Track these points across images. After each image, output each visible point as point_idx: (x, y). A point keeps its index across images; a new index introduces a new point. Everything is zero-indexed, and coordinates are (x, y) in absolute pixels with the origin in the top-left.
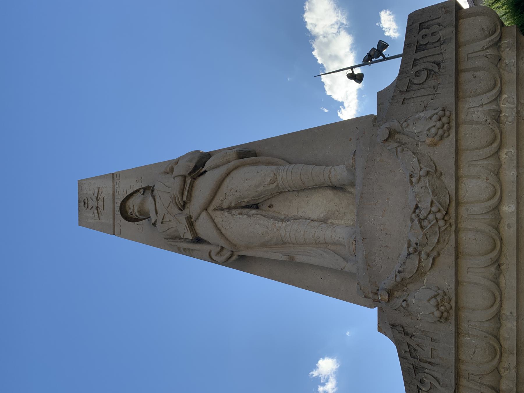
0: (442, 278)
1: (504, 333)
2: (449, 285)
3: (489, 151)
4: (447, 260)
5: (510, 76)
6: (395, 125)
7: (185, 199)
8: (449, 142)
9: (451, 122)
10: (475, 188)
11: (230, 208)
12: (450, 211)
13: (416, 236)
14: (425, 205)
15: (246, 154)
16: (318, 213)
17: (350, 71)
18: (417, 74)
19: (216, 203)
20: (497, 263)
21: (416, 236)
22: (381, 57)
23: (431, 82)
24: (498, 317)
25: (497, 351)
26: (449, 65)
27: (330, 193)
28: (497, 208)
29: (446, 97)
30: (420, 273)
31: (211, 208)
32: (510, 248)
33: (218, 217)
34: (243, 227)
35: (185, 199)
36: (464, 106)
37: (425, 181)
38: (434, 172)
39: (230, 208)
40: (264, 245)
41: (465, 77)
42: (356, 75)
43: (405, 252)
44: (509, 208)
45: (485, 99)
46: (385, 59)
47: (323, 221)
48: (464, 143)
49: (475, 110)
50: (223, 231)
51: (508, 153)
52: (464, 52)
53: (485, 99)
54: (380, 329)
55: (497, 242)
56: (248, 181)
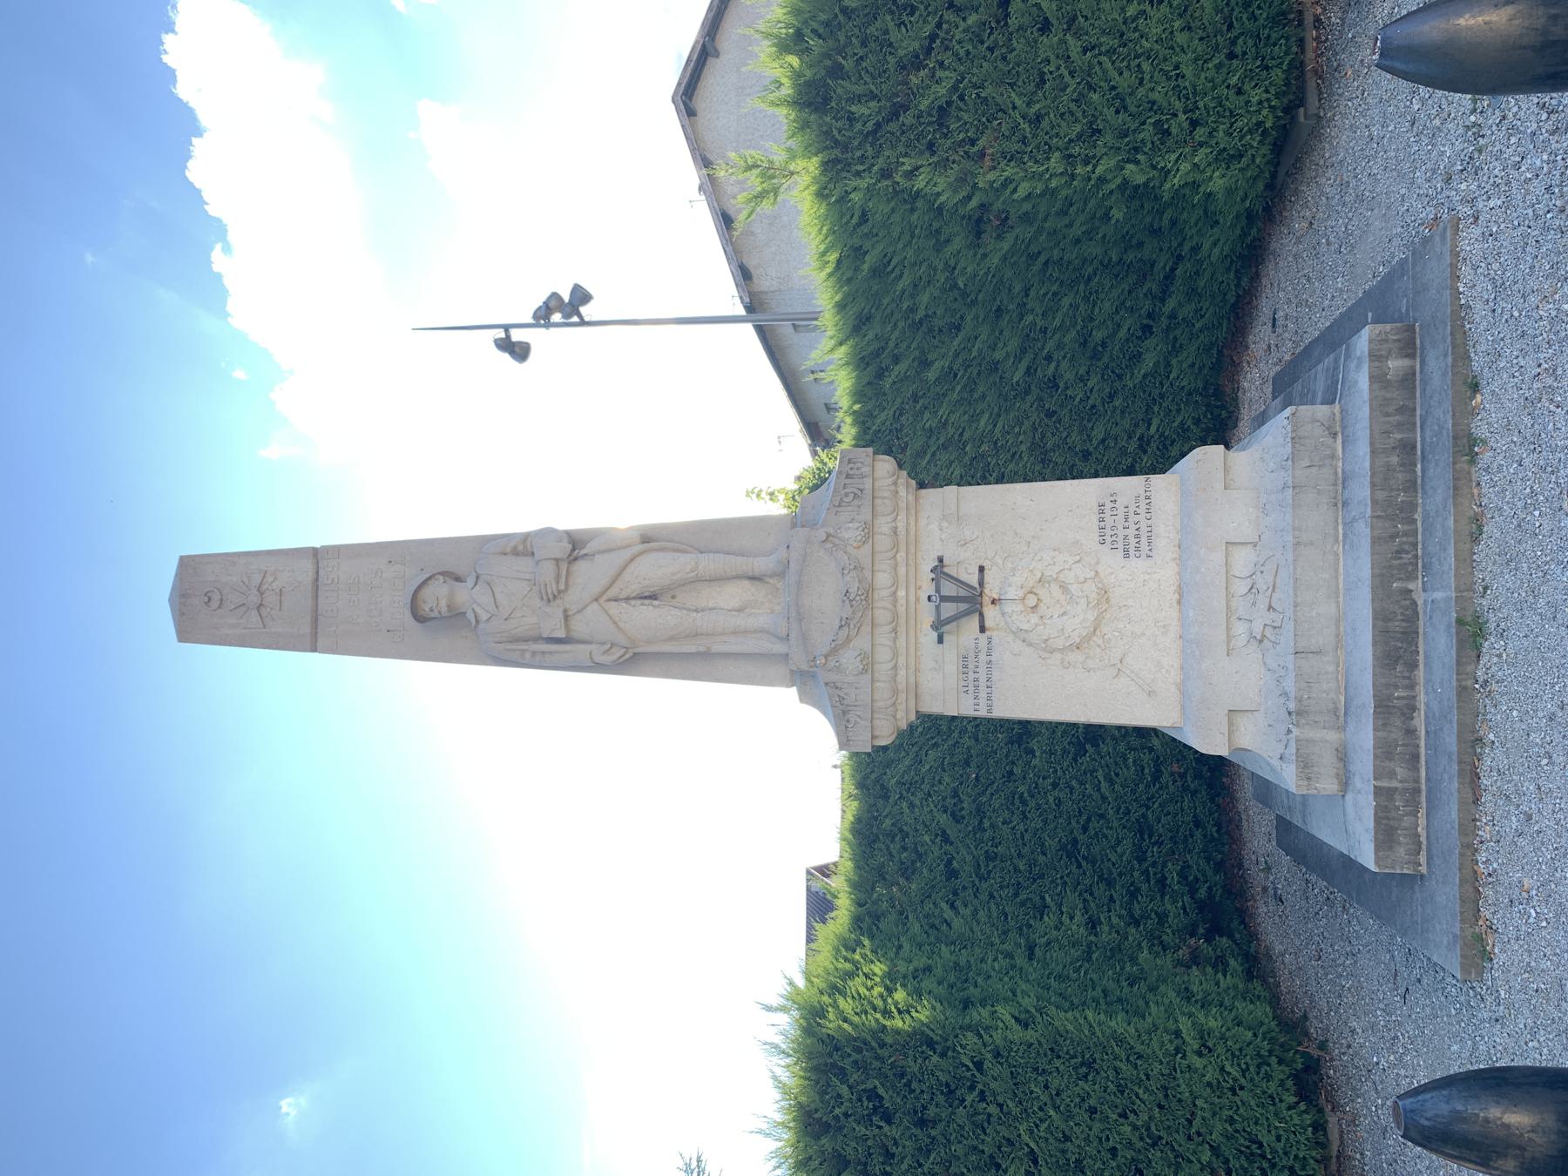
0: (861, 642)
1: (899, 679)
2: (867, 646)
3: (890, 554)
4: (866, 629)
5: (903, 505)
6: (831, 531)
7: (562, 587)
8: (868, 546)
9: (869, 532)
10: (883, 579)
11: (627, 599)
12: (868, 592)
13: (848, 612)
14: (853, 590)
15: (650, 538)
16: (735, 603)
17: (501, 334)
18: (847, 495)
19: (610, 594)
20: (895, 630)
21: (848, 612)
22: (575, 319)
23: (856, 502)
24: (895, 667)
25: (895, 692)
26: (868, 492)
27: (746, 583)
28: (895, 593)
29: (866, 514)
30: (848, 640)
31: (605, 597)
32: (902, 621)
33: (614, 608)
34: (643, 620)
35: (562, 587)
36: (877, 522)
37: (854, 573)
38: (858, 568)
39: (627, 599)
40: (671, 639)
41: (878, 501)
42: (514, 344)
43: (837, 624)
44: (901, 593)
45: (890, 519)
46: (583, 323)
47: (740, 610)
48: (877, 548)
49: (883, 525)
50: (621, 625)
51: (901, 556)
52: (877, 484)
53: (890, 519)
54: (801, 700)
55: (895, 616)
56: (654, 569)
